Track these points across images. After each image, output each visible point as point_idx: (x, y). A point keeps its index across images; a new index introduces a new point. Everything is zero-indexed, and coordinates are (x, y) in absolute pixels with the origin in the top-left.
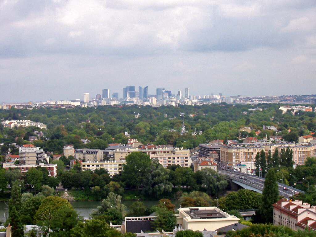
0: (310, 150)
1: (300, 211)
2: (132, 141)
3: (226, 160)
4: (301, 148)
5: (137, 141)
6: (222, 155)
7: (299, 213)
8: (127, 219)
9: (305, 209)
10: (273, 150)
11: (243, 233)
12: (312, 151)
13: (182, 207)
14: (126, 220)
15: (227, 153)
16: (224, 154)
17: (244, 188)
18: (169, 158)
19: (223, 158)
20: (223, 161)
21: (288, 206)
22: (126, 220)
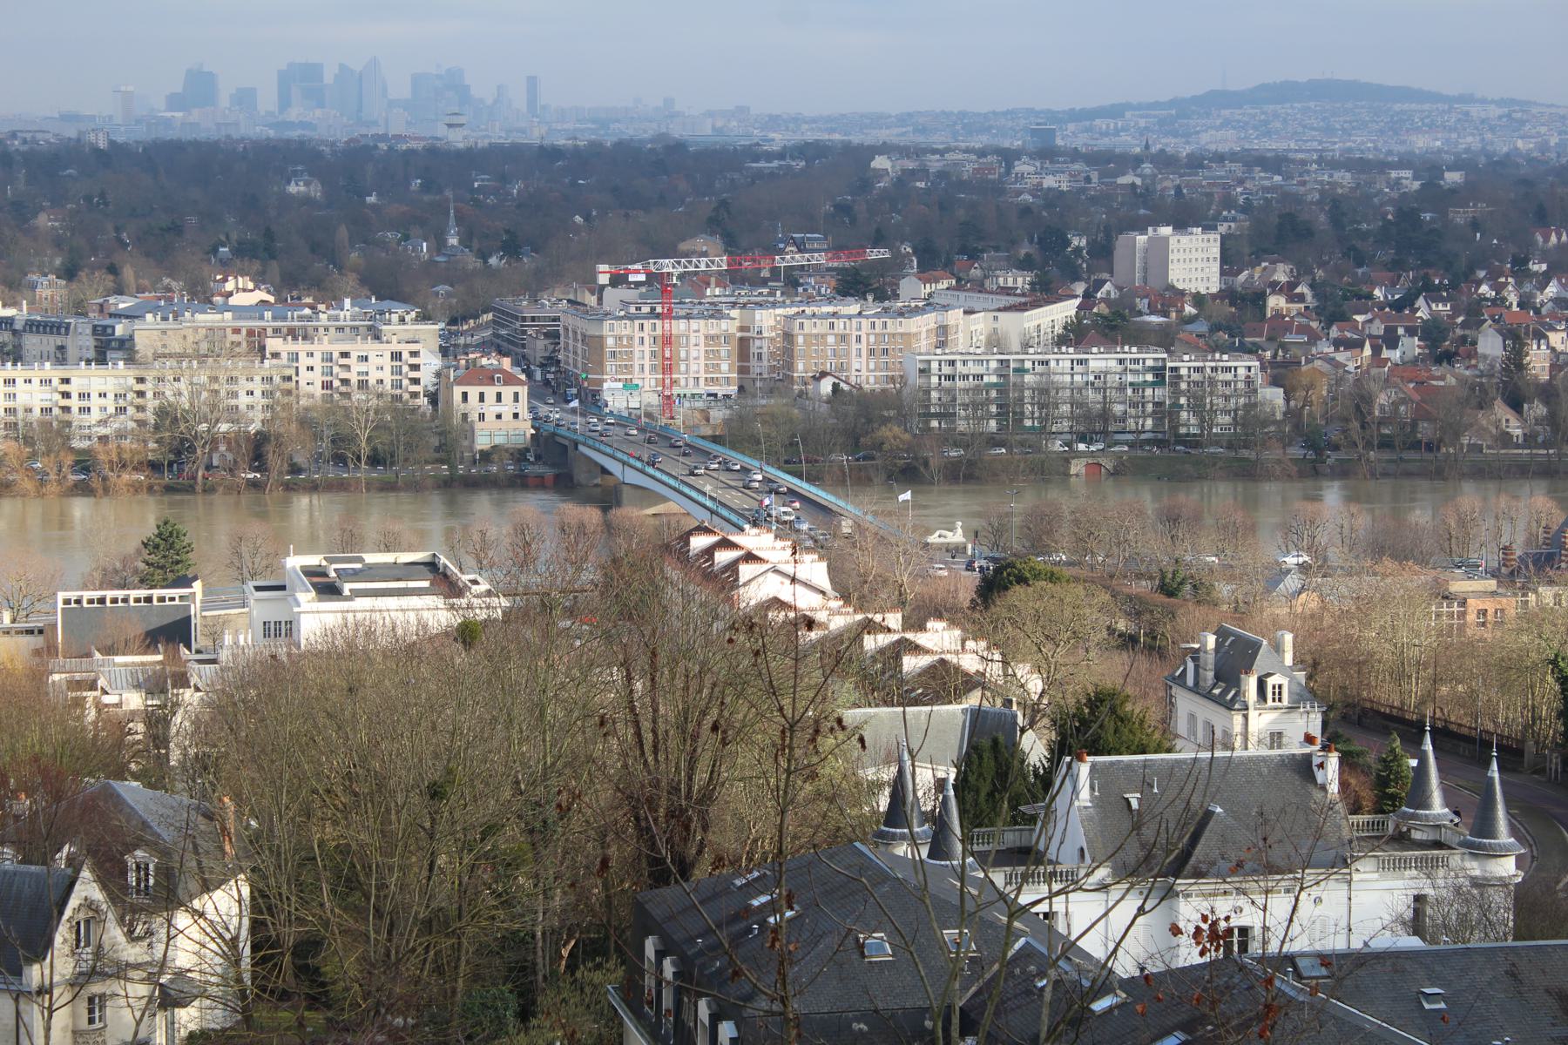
0: (914, 330)
1: (746, 571)
2: (230, 286)
3: (580, 365)
4: (879, 322)
5: (251, 285)
6: (567, 344)
7: (742, 580)
8: (67, 602)
9: (768, 566)
10: (773, 328)
11: (1525, 182)
12: (924, 335)
13: (295, 554)
14: (60, 605)
15: (584, 336)
16: (576, 340)
17: (610, 473)
18: (345, 355)
19: (571, 355)
20: (570, 368)
21: (709, 552)
22: (60, 605)
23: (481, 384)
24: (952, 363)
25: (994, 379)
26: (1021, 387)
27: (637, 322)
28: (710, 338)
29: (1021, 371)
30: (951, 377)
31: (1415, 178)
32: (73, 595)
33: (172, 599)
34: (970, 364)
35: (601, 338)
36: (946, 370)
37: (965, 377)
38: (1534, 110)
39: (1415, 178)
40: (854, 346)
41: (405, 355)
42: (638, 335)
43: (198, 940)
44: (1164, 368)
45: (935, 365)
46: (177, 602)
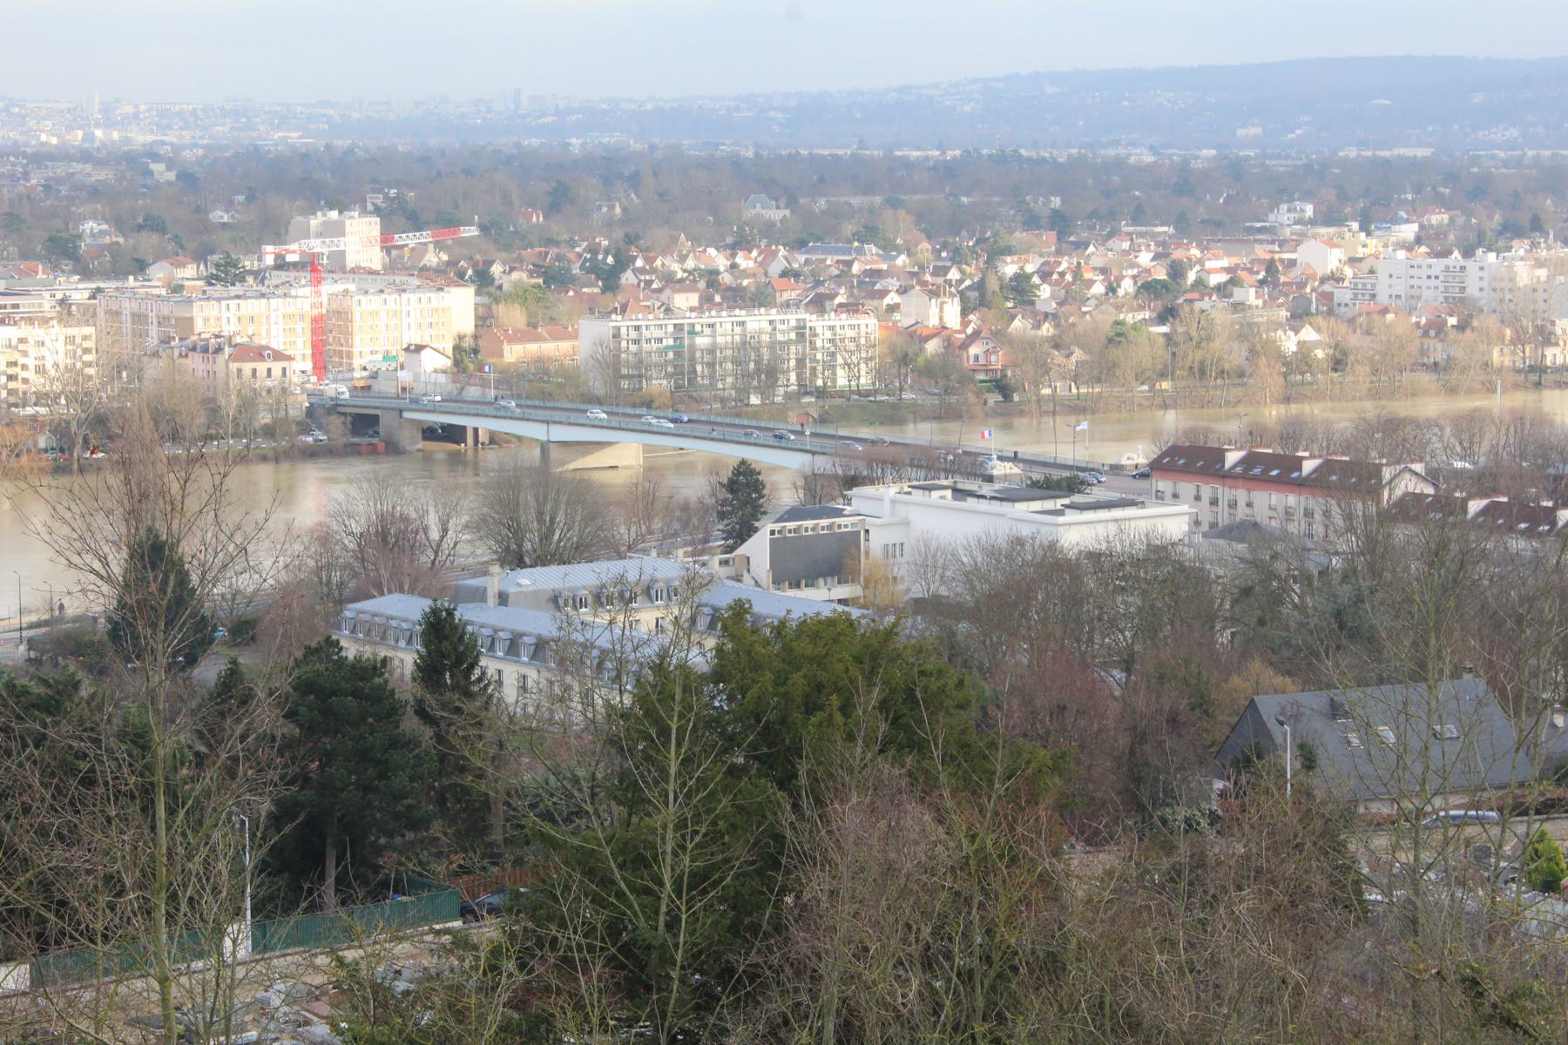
23: (253, 360)
24: (637, 328)
25: (671, 342)
26: (692, 347)
27: (224, 303)
28: (288, 317)
29: (692, 333)
30: (637, 342)
31: (169, 169)
32: (777, 527)
33: (846, 526)
34: (652, 328)
35: (191, 319)
36: (633, 334)
37: (648, 341)
38: (30, 105)
39: (169, 169)
40: (405, 321)
41: (78, 340)
42: (225, 315)
43: (325, 1014)
44: (804, 327)
45: (623, 331)
46: (849, 529)
